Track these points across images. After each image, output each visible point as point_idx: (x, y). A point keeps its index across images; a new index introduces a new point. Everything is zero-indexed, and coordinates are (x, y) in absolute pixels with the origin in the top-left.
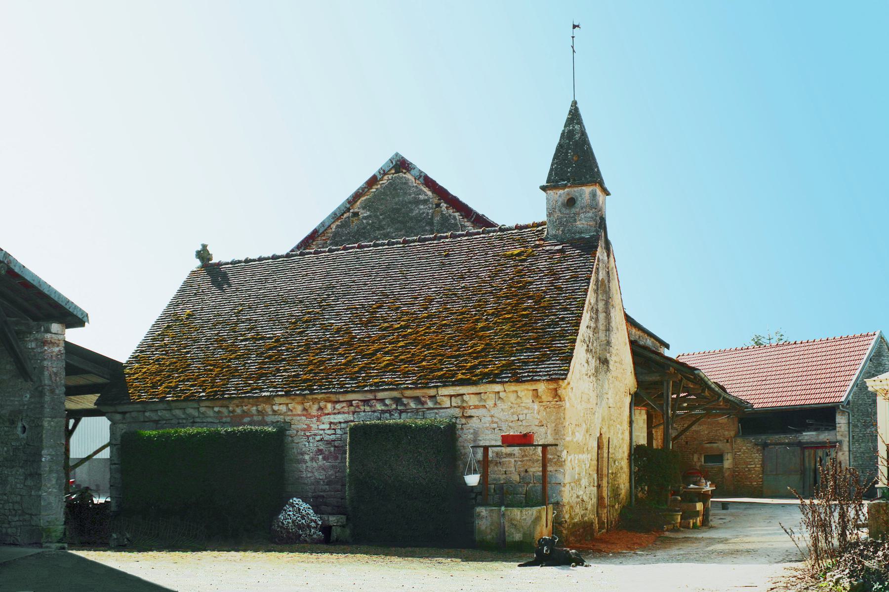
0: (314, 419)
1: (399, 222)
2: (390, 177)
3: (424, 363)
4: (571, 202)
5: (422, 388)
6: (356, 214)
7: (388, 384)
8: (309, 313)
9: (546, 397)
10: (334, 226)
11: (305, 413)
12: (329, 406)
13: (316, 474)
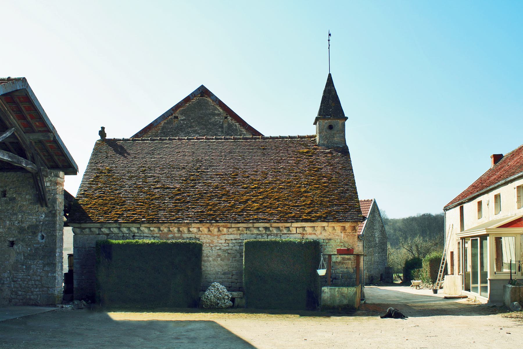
0: (216, 237)
1: (203, 124)
2: (197, 98)
3: (279, 209)
4: (331, 127)
5: (285, 222)
6: (176, 117)
7: (263, 219)
8: (192, 175)
9: (349, 230)
10: (163, 123)
11: (210, 233)
12: (225, 229)
13: (216, 268)
